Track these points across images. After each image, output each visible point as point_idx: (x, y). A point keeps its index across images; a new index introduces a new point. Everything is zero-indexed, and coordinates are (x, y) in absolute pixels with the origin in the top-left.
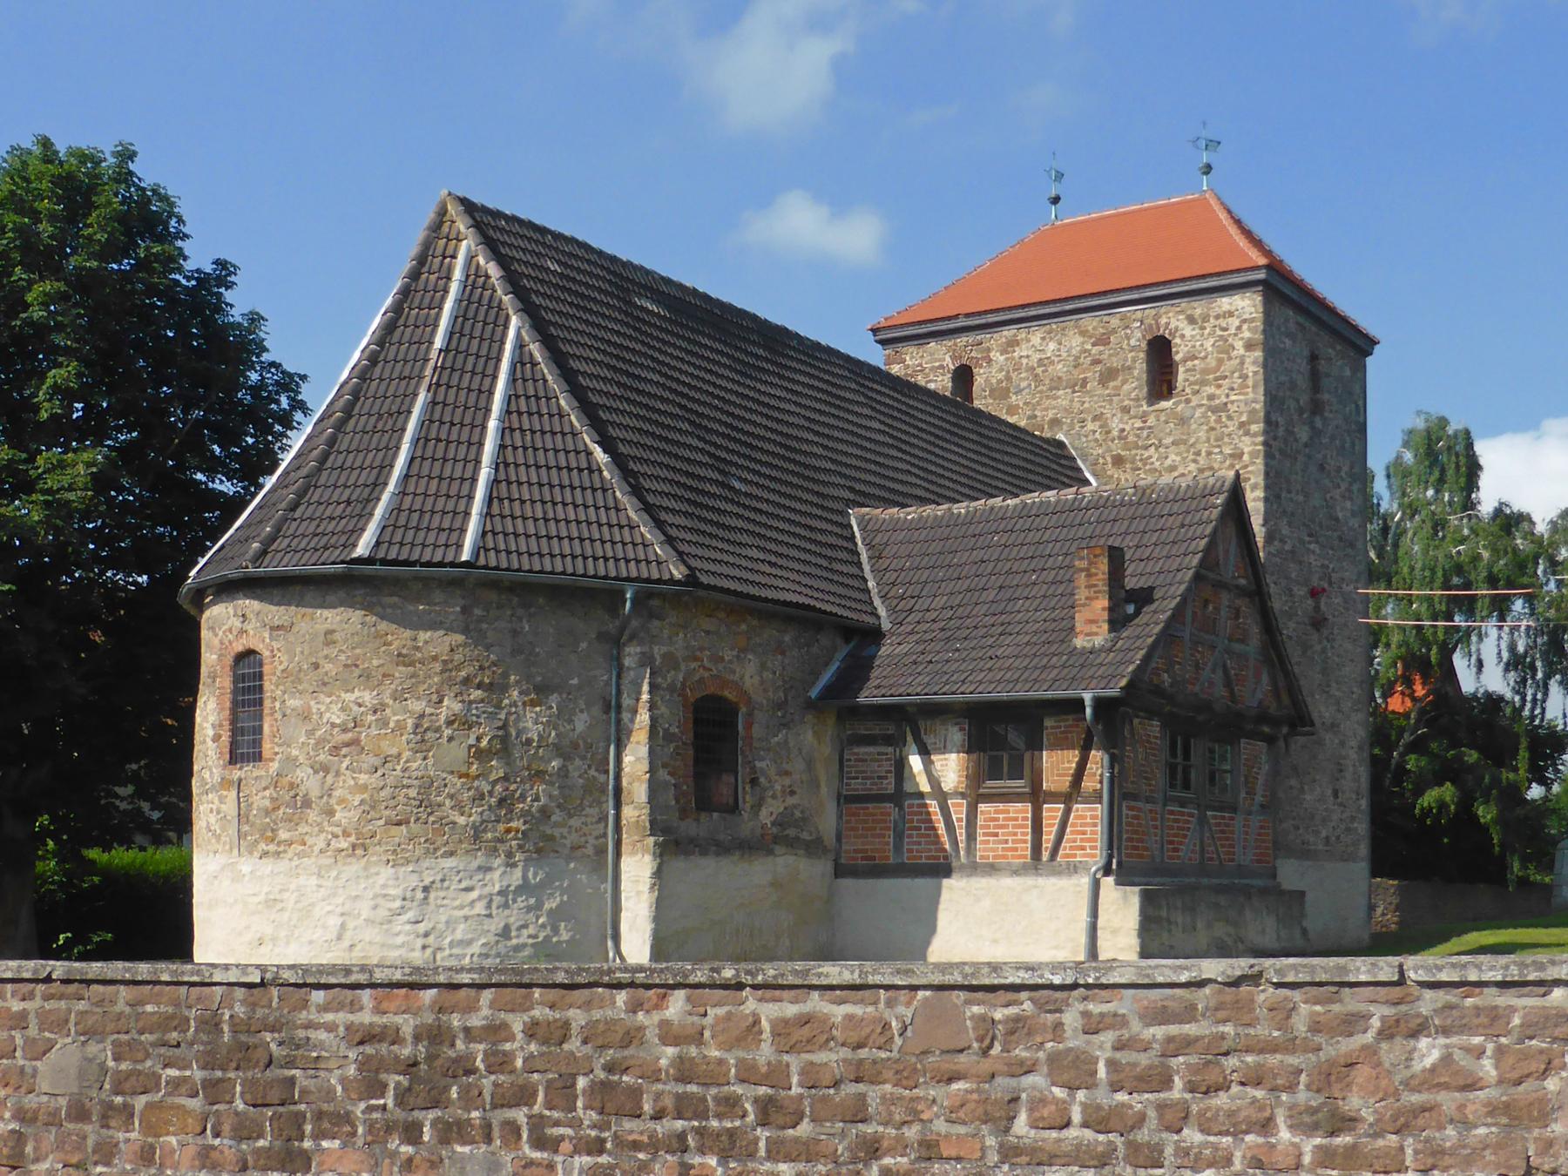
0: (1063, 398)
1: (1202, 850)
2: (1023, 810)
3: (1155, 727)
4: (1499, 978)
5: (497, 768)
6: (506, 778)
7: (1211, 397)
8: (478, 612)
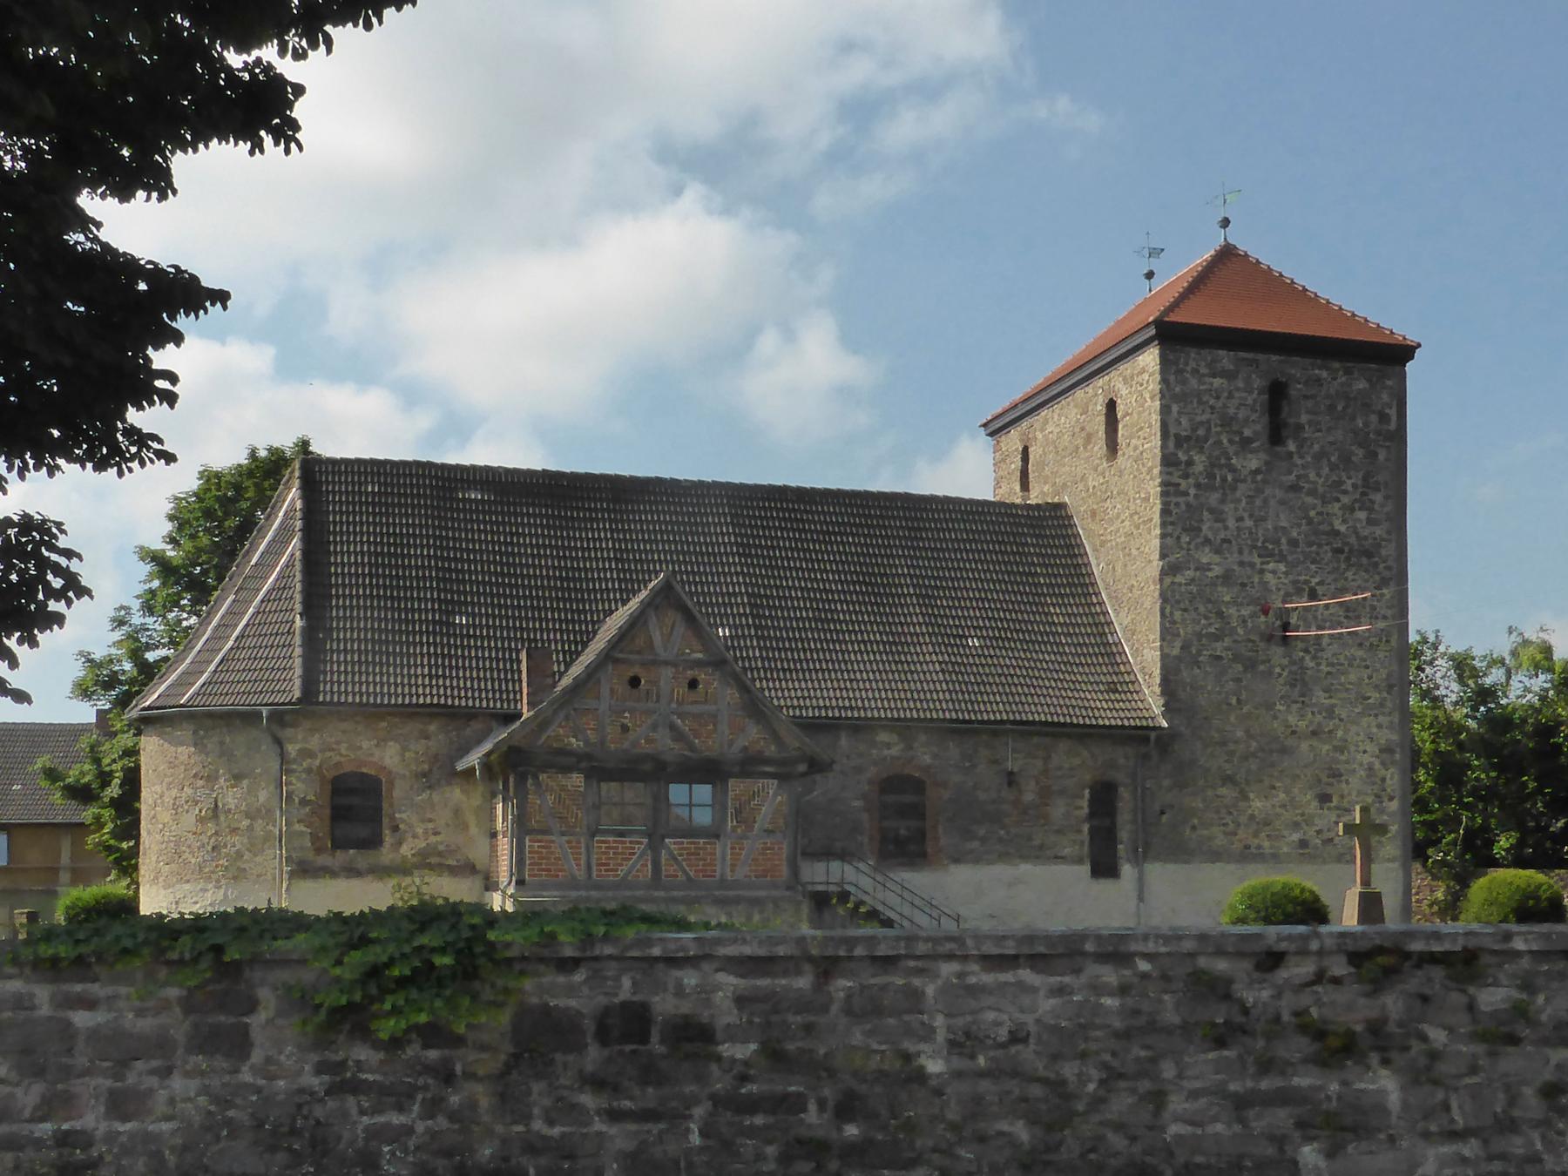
5: (211, 827)
6: (216, 833)
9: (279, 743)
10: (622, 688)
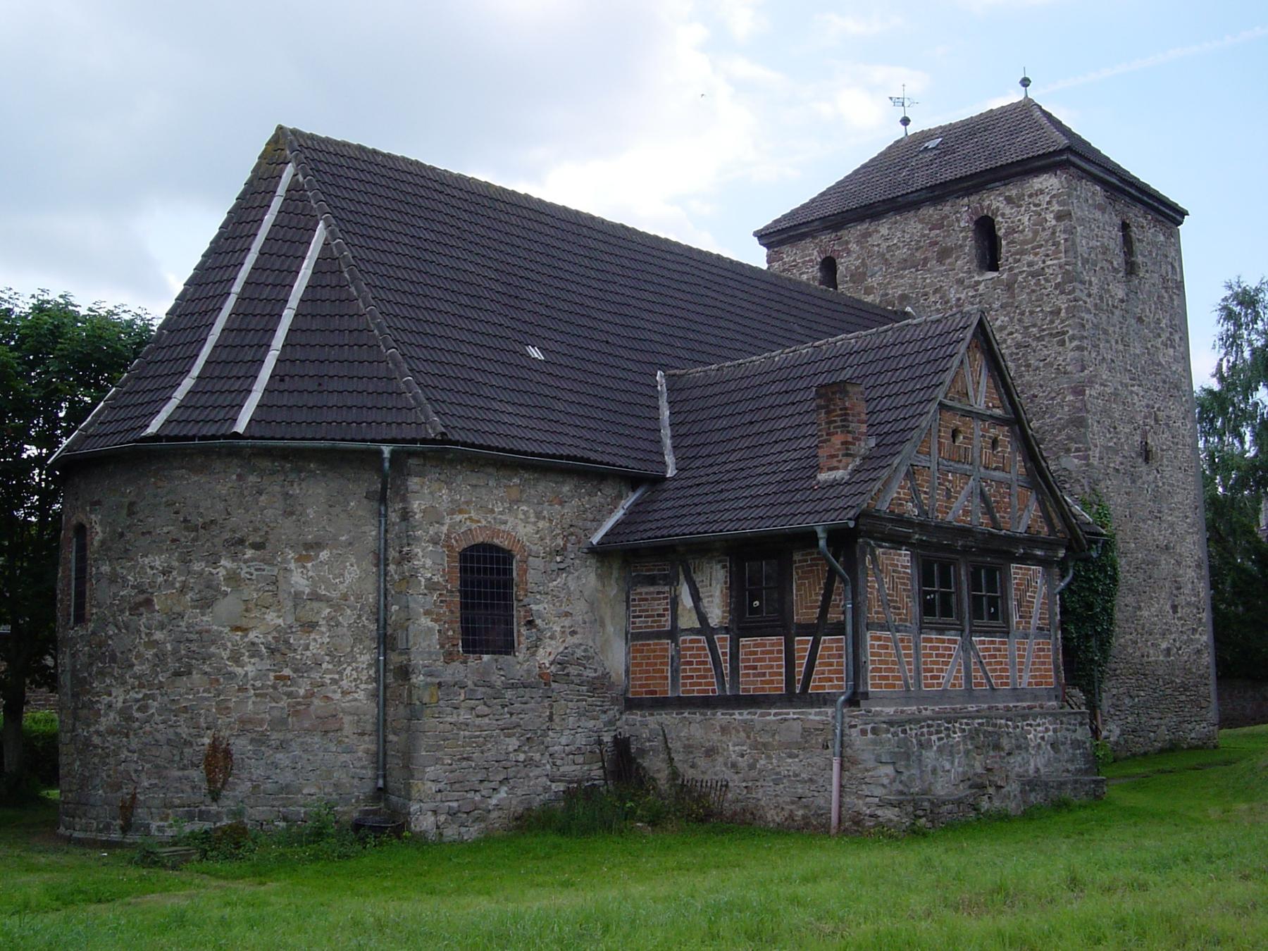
0: (908, 276)
1: (968, 677)
2: (774, 643)
3: (903, 558)
7: (1030, 264)
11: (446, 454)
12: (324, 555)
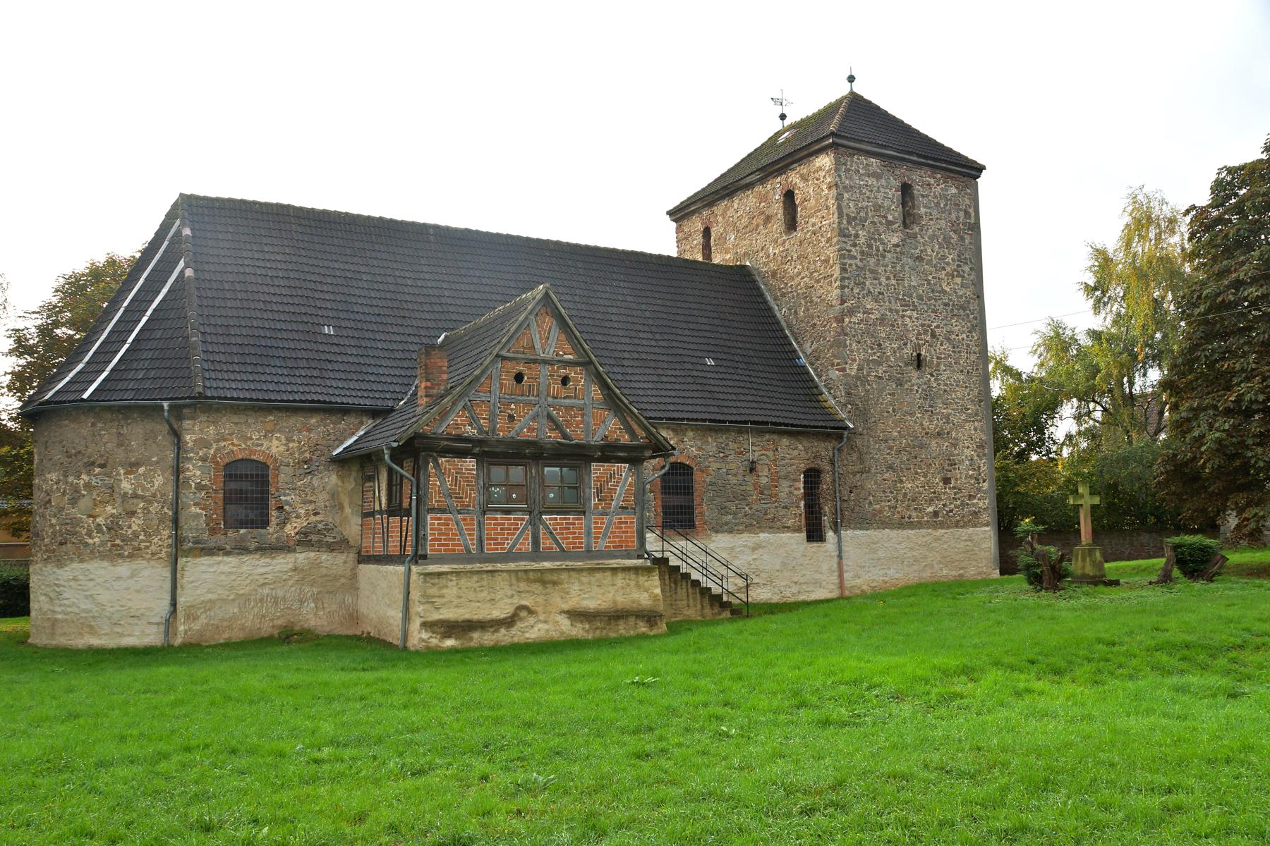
4: (476, 635)
7: (813, 225)
8: (99, 425)
9: (176, 435)
10: (509, 382)
11: (205, 405)
12: (142, 470)
